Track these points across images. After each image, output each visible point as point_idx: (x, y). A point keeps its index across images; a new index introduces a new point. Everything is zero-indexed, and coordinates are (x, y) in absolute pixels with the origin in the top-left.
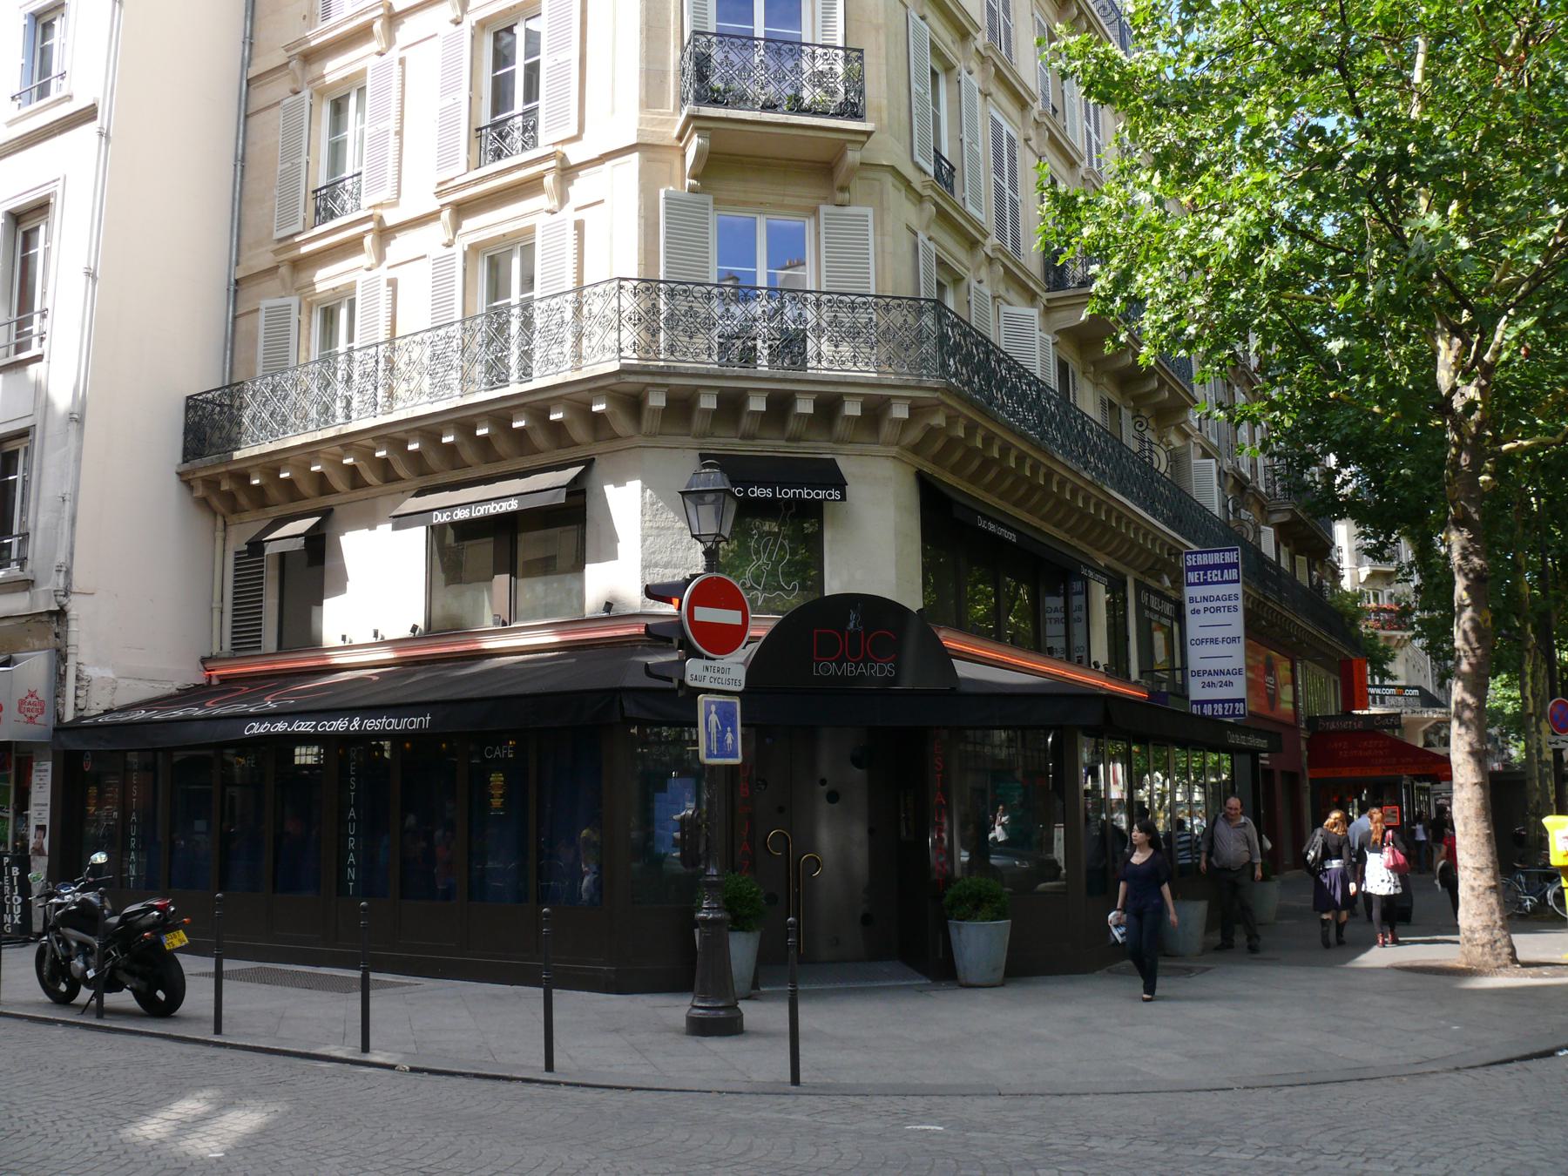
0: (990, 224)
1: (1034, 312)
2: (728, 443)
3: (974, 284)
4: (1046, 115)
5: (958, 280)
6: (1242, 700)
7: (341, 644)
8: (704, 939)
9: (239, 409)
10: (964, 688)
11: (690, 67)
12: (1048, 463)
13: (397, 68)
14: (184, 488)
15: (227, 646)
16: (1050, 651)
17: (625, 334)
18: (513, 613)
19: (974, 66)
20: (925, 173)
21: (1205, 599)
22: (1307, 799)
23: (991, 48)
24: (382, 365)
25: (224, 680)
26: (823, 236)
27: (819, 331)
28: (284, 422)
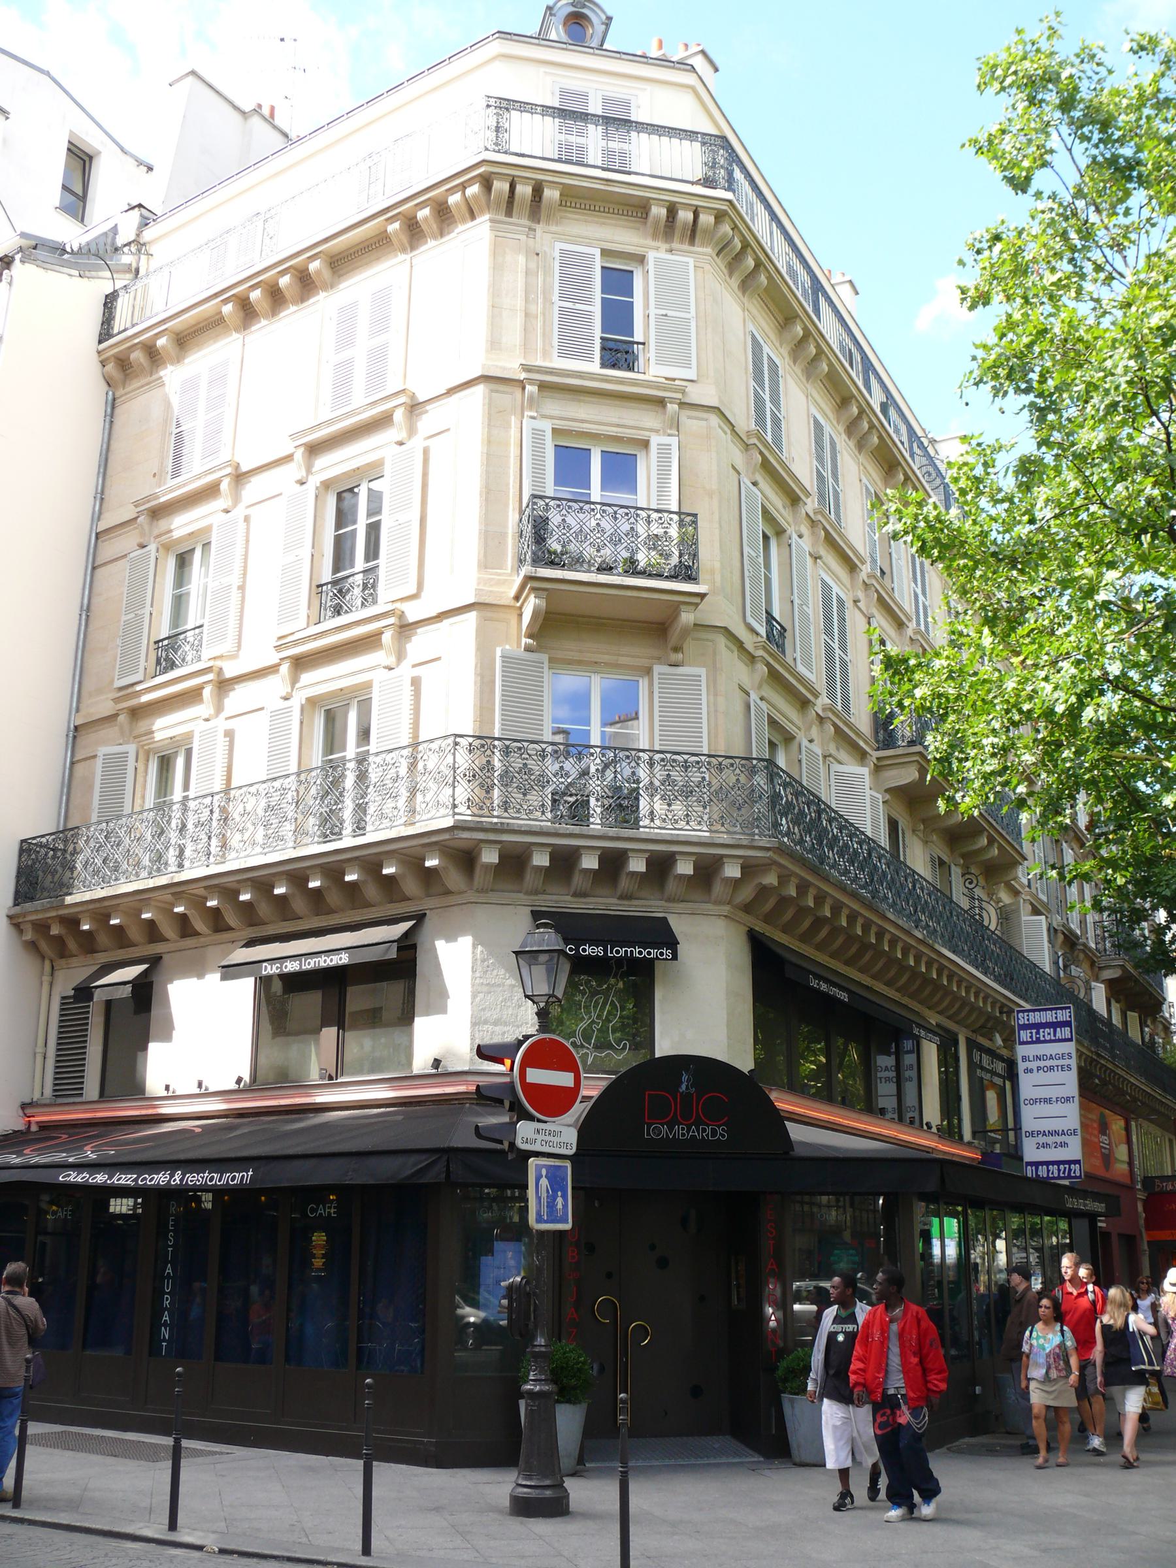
0: (821, 685)
1: (865, 771)
2: (561, 900)
3: (805, 743)
4: (874, 577)
5: (789, 739)
6: (1077, 1162)
7: (165, 1094)
8: (530, 1413)
9: (72, 854)
10: (799, 1152)
11: (528, 530)
12: (880, 922)
13: (242, 526)
14: (12, 929)
15: (48, 1091)
16: (882, 1112)
17: (459, 790)
18: (340, 1066)
19: (804, 529)
20: (757, 634)
21: (1038, 1058)
22: (1145, 1262)
23: (822, 513)
24: (216, 815)
25: (43, 1127)
26: (656, 695)
27: (652, 789)
28: (116, 869)
